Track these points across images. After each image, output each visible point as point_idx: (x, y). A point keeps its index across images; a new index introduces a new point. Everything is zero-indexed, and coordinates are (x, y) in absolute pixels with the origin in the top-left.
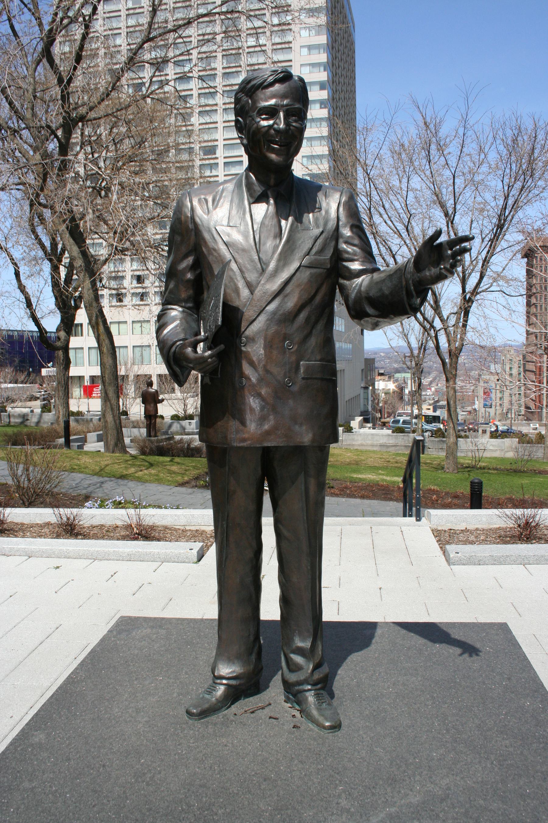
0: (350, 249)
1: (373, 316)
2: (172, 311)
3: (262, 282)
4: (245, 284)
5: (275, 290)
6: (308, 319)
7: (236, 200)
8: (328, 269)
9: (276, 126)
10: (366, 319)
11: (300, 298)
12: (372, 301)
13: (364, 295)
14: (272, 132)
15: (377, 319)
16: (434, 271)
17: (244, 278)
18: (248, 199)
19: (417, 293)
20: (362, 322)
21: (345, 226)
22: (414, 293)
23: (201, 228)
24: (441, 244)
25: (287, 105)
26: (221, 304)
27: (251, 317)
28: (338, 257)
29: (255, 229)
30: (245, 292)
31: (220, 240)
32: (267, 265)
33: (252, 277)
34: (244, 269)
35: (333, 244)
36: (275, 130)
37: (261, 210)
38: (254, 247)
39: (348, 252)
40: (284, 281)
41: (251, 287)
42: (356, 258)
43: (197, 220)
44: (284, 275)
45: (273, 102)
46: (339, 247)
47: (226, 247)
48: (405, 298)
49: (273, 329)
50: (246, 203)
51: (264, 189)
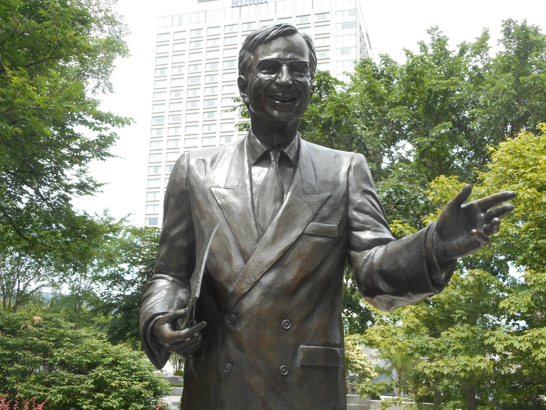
0: (361, 217)
1: (387, 294)
2: (160, 280)
3: (258, 250)
4: (238, 252)
5: (273, 261)
6: (309, 296)
7: (236, 161)
8: (334, 238)
9: (278, 80)
10: (380, 297)
11: (300, 270)
12: (386, 275)
13: (376, 268)
14: (275, 87)
15: (392, 297)
16: (461, 239)
17: (238, 245)
18: (248, 161)
19: (441, 266)
20: (375, 300)
21: (355, 192)
22: (438, 266)
23: (196, 190)
24: (471, 206)
25: (290, 59)
26: (201, 276)
27: (242, 290)
28: (348, 227)
29: (254, 192)
30: (238, 261)
31: (215, 203)
32: (264, 231)
33: (247, 245)
34: (238, 236)
35: (342, 209)
36: (277, 84)
37: (261, 173)
38: (251, 211)
39: (357, 220)
40: (283, 250)
41: (245, 256)
42: (367, 226)
43: (193, 182)
44: (283, 244)
45: (274, 56)
46: (349, 214)
47: (220, 211)
48: (426, 272)
49: (269, 305)
50: (246, 164)
51: (265, 149)
